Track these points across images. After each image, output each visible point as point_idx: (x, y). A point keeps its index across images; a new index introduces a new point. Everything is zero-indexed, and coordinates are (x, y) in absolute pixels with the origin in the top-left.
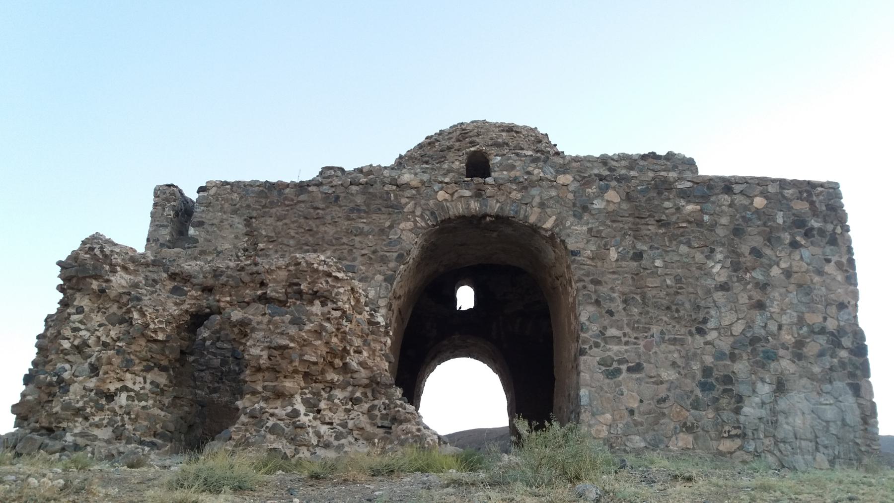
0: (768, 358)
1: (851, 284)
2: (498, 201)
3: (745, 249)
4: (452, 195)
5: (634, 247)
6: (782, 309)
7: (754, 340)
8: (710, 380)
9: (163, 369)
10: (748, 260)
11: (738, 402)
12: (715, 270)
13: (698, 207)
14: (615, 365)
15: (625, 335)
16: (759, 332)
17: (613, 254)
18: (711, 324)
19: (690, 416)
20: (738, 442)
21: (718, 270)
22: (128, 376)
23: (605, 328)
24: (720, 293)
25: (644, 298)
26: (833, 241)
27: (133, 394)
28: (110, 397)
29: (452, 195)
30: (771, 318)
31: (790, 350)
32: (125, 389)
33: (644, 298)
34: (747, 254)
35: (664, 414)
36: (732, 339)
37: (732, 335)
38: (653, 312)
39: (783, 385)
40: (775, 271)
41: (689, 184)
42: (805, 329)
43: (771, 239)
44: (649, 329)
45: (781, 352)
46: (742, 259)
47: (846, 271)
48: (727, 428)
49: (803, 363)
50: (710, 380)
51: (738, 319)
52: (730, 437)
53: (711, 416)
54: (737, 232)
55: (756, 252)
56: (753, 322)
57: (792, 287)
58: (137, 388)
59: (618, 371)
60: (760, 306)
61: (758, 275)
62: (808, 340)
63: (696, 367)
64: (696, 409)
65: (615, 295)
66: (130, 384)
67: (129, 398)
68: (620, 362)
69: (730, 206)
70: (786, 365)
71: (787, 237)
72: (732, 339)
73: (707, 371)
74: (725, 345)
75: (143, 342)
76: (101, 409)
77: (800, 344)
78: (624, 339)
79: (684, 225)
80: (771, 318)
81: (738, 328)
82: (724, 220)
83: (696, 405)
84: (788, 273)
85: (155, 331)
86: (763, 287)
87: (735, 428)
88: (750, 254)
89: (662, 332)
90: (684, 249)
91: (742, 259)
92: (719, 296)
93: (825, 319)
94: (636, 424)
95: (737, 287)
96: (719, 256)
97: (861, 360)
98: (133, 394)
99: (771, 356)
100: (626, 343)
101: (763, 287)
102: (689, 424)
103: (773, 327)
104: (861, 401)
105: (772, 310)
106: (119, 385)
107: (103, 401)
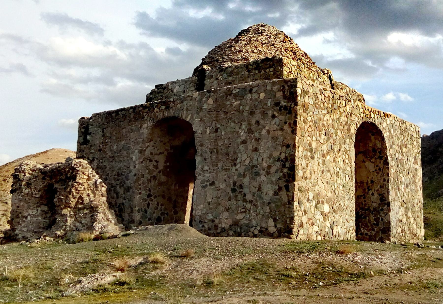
0: (256, 175)
1: (294, 134)
2: (173, 110)
3: (253, 122)
4: (159, 109)
5: (216, 126)
6: (264, 151)
7: (253, 166)
8: (235, 187)
9: (45, 205)
10: (254, 127)
11: (244, 197)
12: (242, 134)
13: (239, 102)
14: (206, 183)
15: (210, 169)
16: (255, 163)
17: (208, 131)
18: (238, 161)
19: (228, 204)
20: (244, 214)
21: (243, 135)
22: (30, 210)
23: (203, 166)
24: (242, 145)
25: (217, 150)
26: (290, 113)
27: (32, 216)
28: (26, 218)
29: (159, 109)
30: (260, 156)
31: (265, 170)
32: (29, 215)
33: (217, 150)
34: (254, 124)
35: (219, 204)
36: (245, 167)
37: (245, 165)
38: (220, 157)
39: (261, 187)
40: (264, 132)
41: (238, 90)
42: (272, 160)
43: (264, 114)
44: (218, 165)
45: (262, 172)
46: (252, 127)
47: (292, 128)
48: (240, 209)
49: (269, 177)
50: (235, 187)
51: (247, 157)
52: (241, 212)
53: (235, 203)
54: (252, 113)
55: (258, 123)
56: (253, 158)
57: (270, 139)
58: (34, 213)
59: (206, 185)
60: (256, 150)
61: (257, 135)
62: (272, 165)
63: (231, 181)
64: (230, 201)
65: (208, 150)
66: (31, 213)
67: (31, 217)
68: (207, 181)
69: (251, 99)
70: (263, 178)
71: (270, 113)
72: (245, 167)
73: (235, 183)
74: (241, 171)
75: (33, 198)
76: (24, 221)
77: (269, 167)
78: (209, 171)
79: (233, 113)
80: (260, 156)
81: (247, 162)
82: (247, 108)
83: (230, 199)
84: (268, 132)
85: (35, 194)
86: (258, 140)
87: (243, 208)
88: (255, 124)
89: (222, 166)
90: (232, 124)
91: (252, 127)
92: (241, 147)
93: (281, 154)
94: (211, 209)
95: (249, 141)
96: (243, 127)
97: (292, 173)
98: (32, 216)
99: (258, 174)
100: (210, 173)
101: (258, 140)
102: (227, 208)
103: (260, 160)
104: (288, 193)
105: (260, 151)
106: (27, 214)
107: (24, 219)
